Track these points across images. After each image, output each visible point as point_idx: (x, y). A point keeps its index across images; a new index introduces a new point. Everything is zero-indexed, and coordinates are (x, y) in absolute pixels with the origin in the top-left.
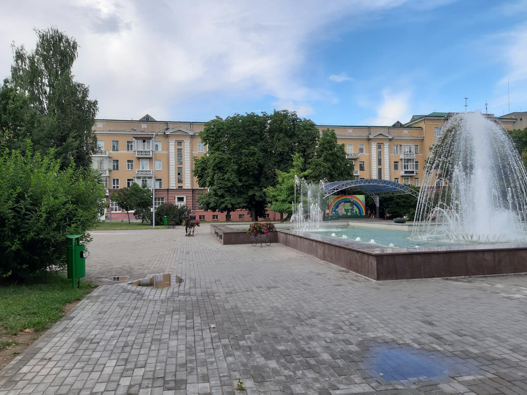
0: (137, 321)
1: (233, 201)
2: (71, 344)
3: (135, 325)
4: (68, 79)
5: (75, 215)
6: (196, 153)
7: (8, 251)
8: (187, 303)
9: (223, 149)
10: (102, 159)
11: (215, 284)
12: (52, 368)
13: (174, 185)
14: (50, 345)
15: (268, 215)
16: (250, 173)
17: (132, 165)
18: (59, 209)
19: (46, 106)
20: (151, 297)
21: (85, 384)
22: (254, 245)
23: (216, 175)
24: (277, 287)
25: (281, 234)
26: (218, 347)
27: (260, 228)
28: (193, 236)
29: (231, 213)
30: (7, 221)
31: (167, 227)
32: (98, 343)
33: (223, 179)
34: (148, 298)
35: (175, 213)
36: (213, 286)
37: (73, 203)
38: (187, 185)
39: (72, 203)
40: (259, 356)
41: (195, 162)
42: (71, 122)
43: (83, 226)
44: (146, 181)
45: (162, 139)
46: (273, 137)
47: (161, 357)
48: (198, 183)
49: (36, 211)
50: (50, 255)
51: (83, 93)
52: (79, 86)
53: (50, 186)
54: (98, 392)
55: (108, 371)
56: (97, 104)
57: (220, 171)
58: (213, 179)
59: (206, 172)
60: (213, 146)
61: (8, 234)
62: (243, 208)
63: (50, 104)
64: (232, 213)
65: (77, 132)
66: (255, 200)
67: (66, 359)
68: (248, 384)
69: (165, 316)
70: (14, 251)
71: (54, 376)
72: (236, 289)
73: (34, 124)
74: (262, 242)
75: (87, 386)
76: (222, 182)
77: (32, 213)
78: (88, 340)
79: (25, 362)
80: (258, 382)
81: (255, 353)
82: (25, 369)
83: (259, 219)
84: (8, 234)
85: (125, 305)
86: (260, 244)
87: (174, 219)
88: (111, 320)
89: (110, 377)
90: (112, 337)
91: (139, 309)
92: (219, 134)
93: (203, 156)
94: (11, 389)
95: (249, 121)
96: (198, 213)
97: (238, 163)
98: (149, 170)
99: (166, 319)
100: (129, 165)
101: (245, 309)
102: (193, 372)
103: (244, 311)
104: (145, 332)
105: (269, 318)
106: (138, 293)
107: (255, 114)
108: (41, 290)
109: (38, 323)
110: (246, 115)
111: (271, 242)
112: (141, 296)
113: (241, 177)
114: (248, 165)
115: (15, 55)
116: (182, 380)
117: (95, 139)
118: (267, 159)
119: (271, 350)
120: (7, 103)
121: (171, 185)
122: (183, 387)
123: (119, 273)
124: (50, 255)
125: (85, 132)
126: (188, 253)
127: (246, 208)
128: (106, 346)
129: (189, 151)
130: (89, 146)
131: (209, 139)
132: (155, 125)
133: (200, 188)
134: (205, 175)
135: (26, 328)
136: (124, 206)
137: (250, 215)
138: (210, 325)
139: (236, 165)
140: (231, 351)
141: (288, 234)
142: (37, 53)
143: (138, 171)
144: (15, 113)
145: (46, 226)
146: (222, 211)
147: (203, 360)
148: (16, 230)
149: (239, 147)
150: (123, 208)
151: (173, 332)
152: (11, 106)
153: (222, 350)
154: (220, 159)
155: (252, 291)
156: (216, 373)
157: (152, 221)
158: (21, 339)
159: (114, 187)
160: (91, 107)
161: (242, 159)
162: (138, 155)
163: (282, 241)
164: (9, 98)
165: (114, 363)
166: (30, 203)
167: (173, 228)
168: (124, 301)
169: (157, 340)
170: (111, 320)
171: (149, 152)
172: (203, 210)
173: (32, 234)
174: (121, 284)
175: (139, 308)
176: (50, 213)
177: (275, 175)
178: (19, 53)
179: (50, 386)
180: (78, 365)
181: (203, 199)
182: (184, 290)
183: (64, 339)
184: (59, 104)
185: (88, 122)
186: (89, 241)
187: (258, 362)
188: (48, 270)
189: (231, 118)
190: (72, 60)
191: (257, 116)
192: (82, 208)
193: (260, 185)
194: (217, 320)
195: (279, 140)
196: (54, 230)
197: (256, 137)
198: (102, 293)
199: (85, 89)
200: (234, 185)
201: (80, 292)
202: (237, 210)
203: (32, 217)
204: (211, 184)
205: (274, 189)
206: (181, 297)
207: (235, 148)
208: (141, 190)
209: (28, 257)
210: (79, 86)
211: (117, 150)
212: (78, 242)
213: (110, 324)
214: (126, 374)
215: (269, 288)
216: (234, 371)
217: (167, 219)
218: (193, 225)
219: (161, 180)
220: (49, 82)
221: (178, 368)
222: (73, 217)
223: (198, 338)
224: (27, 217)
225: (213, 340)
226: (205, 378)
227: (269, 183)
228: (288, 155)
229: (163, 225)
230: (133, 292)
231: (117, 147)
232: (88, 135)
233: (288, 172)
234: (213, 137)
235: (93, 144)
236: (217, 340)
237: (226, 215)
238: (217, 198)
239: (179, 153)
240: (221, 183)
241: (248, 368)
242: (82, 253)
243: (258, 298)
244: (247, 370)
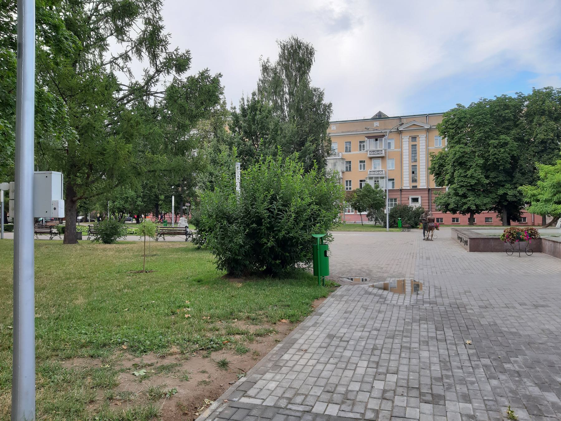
0: (383, 325)
1: (478, 202)
2: (323, 339)
3: (382, 329)
4: (305, 84)
5: (318, 215)
6: (432, 148)
7: (264, 247)
8: (434, 313)
9: (464, 141)
10: (335, 161)
11: (465, 296)
12: (309, 360)
13: (408, 185)
14: (305, 337)
15: (525, 218)
16: (500, 167)
17: (364, 165)
18: (305, 210)
19: (287, 114)
20: (394, 302)
21: (340, 380)
22: (510, 253)
23: (457, 172)
24: (548, 306)
25: (547, 242)
26: (477, 367)
27: (518, 233)
28: (431, 240)
29: (475, 216)
30: (263, 220)
31: (402, 229)
32: (348, 342)
33: (465, 176)
34: (391, 302)
35: (410, 215)
36: (462, 297)
37: (317, 204)
38: (422, 184)
39: (316, 204)
40: (530, 384)
41: (431, 158)
42: (308, 127)
43: (326, 226)
44: (378, 181)
45: (394, 136)
46: (532, 121)
47: (413, 367)
48: (435, 181)
49: (286, 212)
50: (298, 253)
51: (319, 97)
52: (315, 91)
53: (298, 189)
54: (353, 391)
55: (360, 371)
56: (331, 106)
57: (461, 167)
58: (452, 176)
59: (444, 168)
60: (453, 139)
61: (264, 232)
62: (490, 210)
63: (290, 111)
64: (476, 216)
65: (314, 136)
66: (507, 201)
67: (320, 352)
68: (520, 414)
69: (411, 324)
70: (269, 248)
71: (311, 368)
72: (492, 303)
73: (277, 131)
74: (520, 251)
75: (341, 382)
76: (464, 179)
77: (283, 213)
78: (338, 338)
79: (285, 350)
80: (534, 415)
81: (525, 380)
82: (286, 357)
83: (512, 223)
84: (264, 232)
85: (369, 308)
86: (517, 254)
87: (409, 222)
88: (357, 320)
89: (363, 377)
90: (360, 338)
91: (384, 313)
92: (460, 124)
93: (441, 151)
94: (278, 373)
95: (499, 106)
96: (436, 214)
97: (484, 157)
98: (381, 170)
99: (413, 327)
100: (361, 165)
101: (507, 327)
102: (451, 388)
103: (506, 329)
104: (393, 337)
105: (541, 342)
106: (381, 296)
107: (507, 96)
108: (291, 284)
109: (292, 316)
110: (495, 99)
111: (533, 251)
112: (383, 300)
113: (489, 173)
114: (497, 159)
115: (261, 68)
116: (440, 395)
117: (330, 141)
118: (524, 148)
119: (547, 380)
120: (256, 114)
121: (404, 185)
122: (442, 402)
123: (358, 274)
124: (298, 253)
125: (321, 136)
126: (428, 258)
127: (494, 210)
128: (355, 346)
129: (424, 147)
130: (324, 148)
131: (448, 132)
132: (387, 121)
133: (437, 187)
134: (443, 172)
135: (282, 319)
136: (358, 208)
137: (500, 218)
138: (465, 340)
139: (482, 159)
140: (494, 374)
141: (557, 242)
142: (278, 64)
143: (370, 171)
144: (262, 123)
145: (295, 225)
146: (464, 213)
147: (462, 378)
148: (271, 228)
149: (486, 137)
150: (356, 209)
151: (423, 342)
152: (258, 117)
153: (483, 370)
154: (461, 153)
155: (514, 308)
156: (479, 394)
157: (385, 223)
158: (280, 328)
159: (347, 188)
160: (326, 110)
161: (489, 152)
162: (370, 154)
163: (549, 251)
164: (256, 110)
165: (365, 364)
166: (282, 204)
167: (408, 231)
168: (368, 304)
169: (406, 348)
170: (357, 320)
171: (382, 151)
172: (441, 212)
173: (283, 233)
174: (362, 286)
175: (383, 312)
176: (298, 213)
177: (535, 169)
178: (265, 65)
179: (309, 376)
180: (332, 360)
181: (441, 199)
182: (429, 299)
183: (316, 333)
184: (298, 110)
185: (323, 125)
186: (331, 241)
187: (531, 391)
188: (296, 266)
189: (475, 104)
190: (309, 65)
191: (510, 98)
192: (324, 209)
193: (513, 182)
194: (472, 336)
195: (540, 125)
196: (302, 229)
197: (508, 123)
198: (345, 293)
199: (321, 93)
200: (479, 182)
201: (325, 290)
202: (483, 212)
203: (283, 217)
204: (451, 182)
205: (533, 188)
206: (427, 306)
207: (480, 139)
208: (374, 191)
209: (280, 254)
210: (315, 91)
211: (350, 151)
212: (322, 241)
213: (357, 324)
214: (378, 377)
215: (536, 306)
216: (501, 396)
217: (401, 221)
218: (431, 229)
219: (393, 180)
220: (289, 90)
221: (433, 381)
222: (317, 217)
223: (452, 353)
224: (280, 217)
225: (470, 357)
226: (467, 399)
227: (526, 179)
228: (554, 143)
229: (397, 227)
230: (375, 295)
231: (350, 148)
232: (323, 138)
233: (553, 165)
234: (453, 128)
235: (328, 146)
236: (475, 359)
237: (469, 219)
238: (458, 198)
239: (414, 149)
240: (462, 181)
241: (518, 396)
242: (325, 252)
243: (523, 317)
244: (517, 398)
